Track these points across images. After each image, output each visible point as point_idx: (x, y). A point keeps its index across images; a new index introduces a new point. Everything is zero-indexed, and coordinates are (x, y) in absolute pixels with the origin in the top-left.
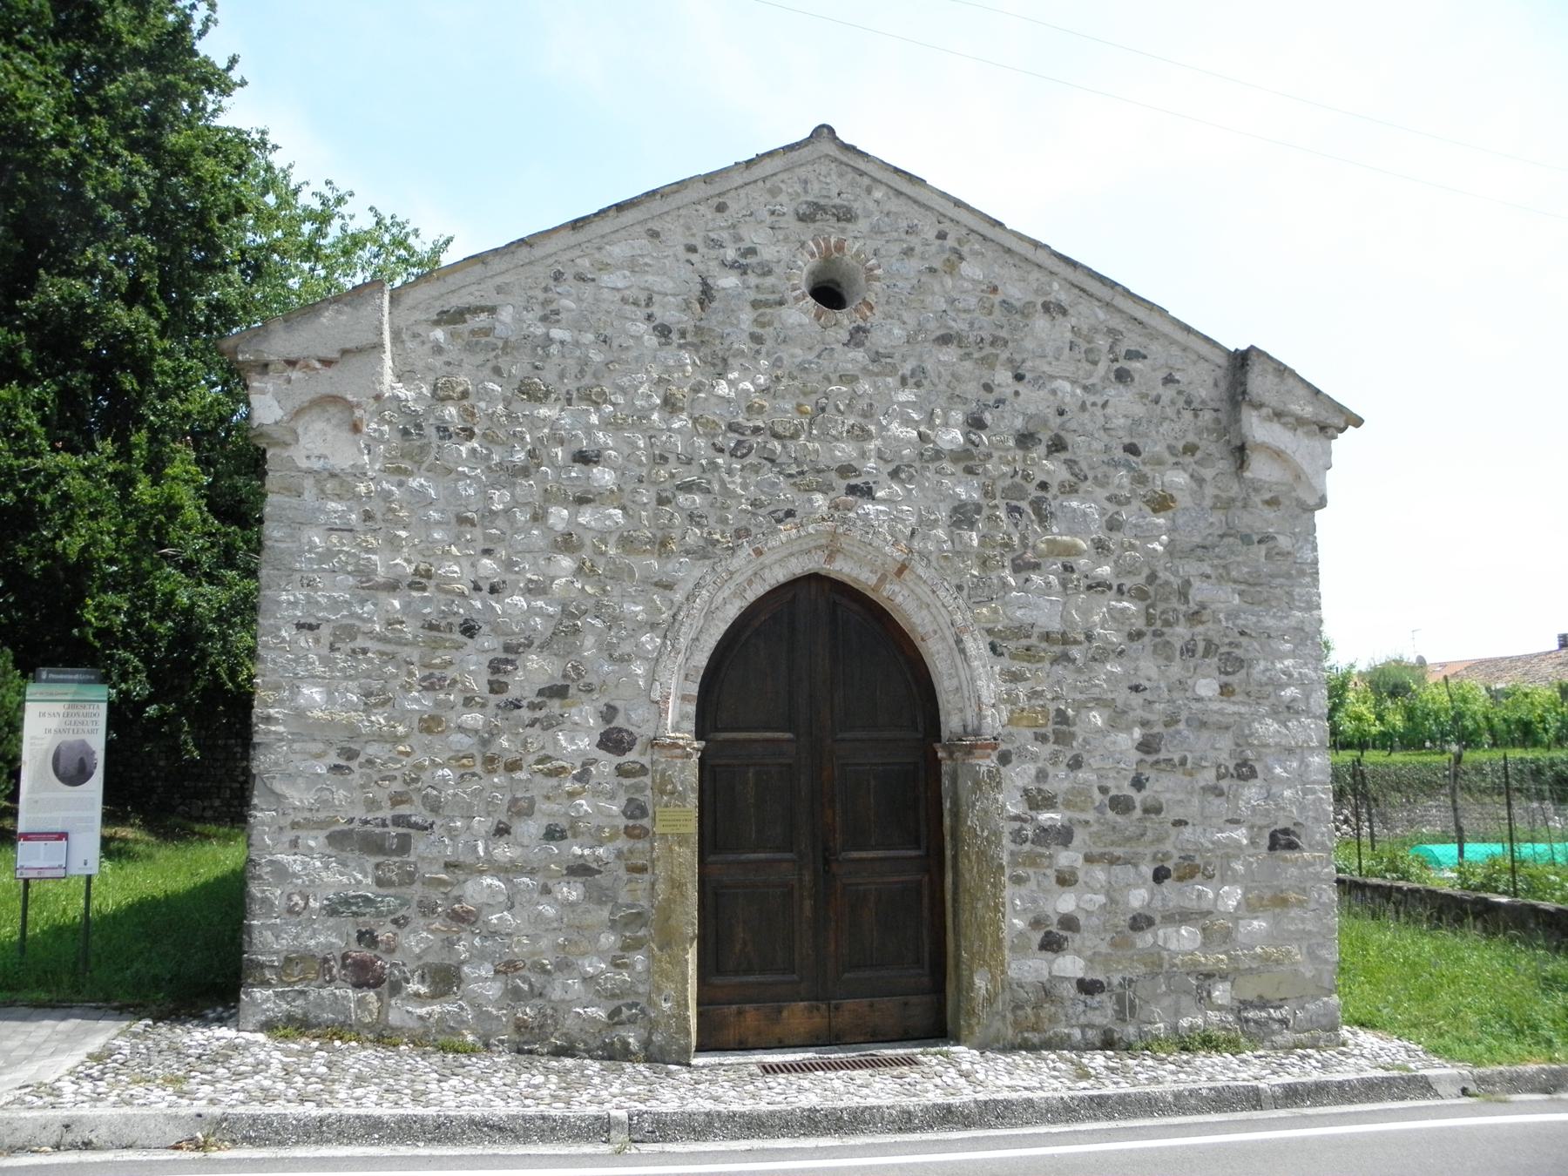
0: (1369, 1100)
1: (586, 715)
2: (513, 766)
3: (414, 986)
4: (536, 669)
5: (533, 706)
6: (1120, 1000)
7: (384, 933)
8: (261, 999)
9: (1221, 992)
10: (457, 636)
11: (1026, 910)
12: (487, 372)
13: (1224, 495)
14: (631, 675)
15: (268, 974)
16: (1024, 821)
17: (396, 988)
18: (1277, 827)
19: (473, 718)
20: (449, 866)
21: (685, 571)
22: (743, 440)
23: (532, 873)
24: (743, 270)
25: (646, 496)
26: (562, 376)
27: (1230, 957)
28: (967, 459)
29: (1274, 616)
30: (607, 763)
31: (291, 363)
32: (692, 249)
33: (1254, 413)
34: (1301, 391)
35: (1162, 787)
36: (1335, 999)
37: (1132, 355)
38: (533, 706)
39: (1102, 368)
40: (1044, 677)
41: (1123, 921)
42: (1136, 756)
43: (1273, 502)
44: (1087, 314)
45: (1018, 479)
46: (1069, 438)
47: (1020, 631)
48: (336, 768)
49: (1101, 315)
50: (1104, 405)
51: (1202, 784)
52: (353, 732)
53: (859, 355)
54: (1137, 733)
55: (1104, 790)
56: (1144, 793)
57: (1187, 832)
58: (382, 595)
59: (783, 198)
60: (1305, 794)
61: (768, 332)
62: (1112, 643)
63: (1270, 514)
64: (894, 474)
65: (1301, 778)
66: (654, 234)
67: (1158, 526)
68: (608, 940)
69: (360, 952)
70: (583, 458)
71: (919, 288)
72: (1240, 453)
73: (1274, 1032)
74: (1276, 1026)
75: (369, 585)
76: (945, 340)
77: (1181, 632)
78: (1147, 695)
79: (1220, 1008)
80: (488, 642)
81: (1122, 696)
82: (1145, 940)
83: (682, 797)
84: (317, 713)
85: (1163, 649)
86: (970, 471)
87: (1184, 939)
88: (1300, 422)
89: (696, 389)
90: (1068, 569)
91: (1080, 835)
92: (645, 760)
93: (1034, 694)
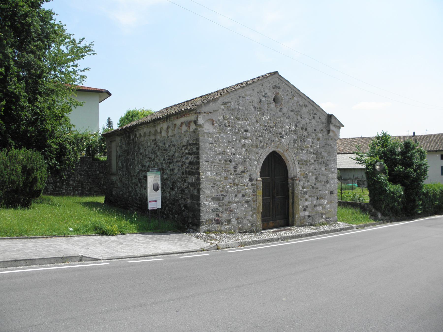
1: (247, 175)
2: (237, 185)
3: (225, 223)
4: (240, 168)
5: (240, 174)
7: (220, 215)
8: (203, 228)
10: (229, 162)
11: (303, 204)
12: (231, 114)
14: (253, 169)
15: (204, 223)
17: (222, 224)
19: (232, 177)
20: (229, 202)
21: (260, 150)
22: (267, 128)
23: (240, 203)
24: (265, 97)
25: (254, 138)
26: (242, 116)
28: (295, 132)
30: (250, 184)
31: (205, 112)
32: (258, 93)
35: (318, 185)
36: (337, 217)
37: (315, 114)
38: (240, 174)
39: (311, 116)
40: (304, 167)
41: (313, 206)
42: (315, 180)
43: (332, 139)
44: (310, 107)
46: (308, 128)
47: (302, 160)
48: (212, 186)
52: (215, 180)
53: (281, 113)
55: (311, 185)
58: (218, 155)
59: (271, 84)
61: (269, 109)
63: (331, 141)
64: (286, 134)
65: (334, 183)
66: (253, 90)
68: (251, 213)
69: (217, 218)
70: (246, 131)
71: (288, 102)
72: (329, 131)
75: (216, 154)
76: (292, 111)
80: (234, 163)
81: (313, 170)
82: (315, 209)
83: (260, 189)
84: (209, 177)
85: (318, 163)
86: (295, 134)
87: (320, 208)
89: (260, 119)
90: (308, 150)
91: (308, 193)
92: (255, 183)
93: (304, 170)
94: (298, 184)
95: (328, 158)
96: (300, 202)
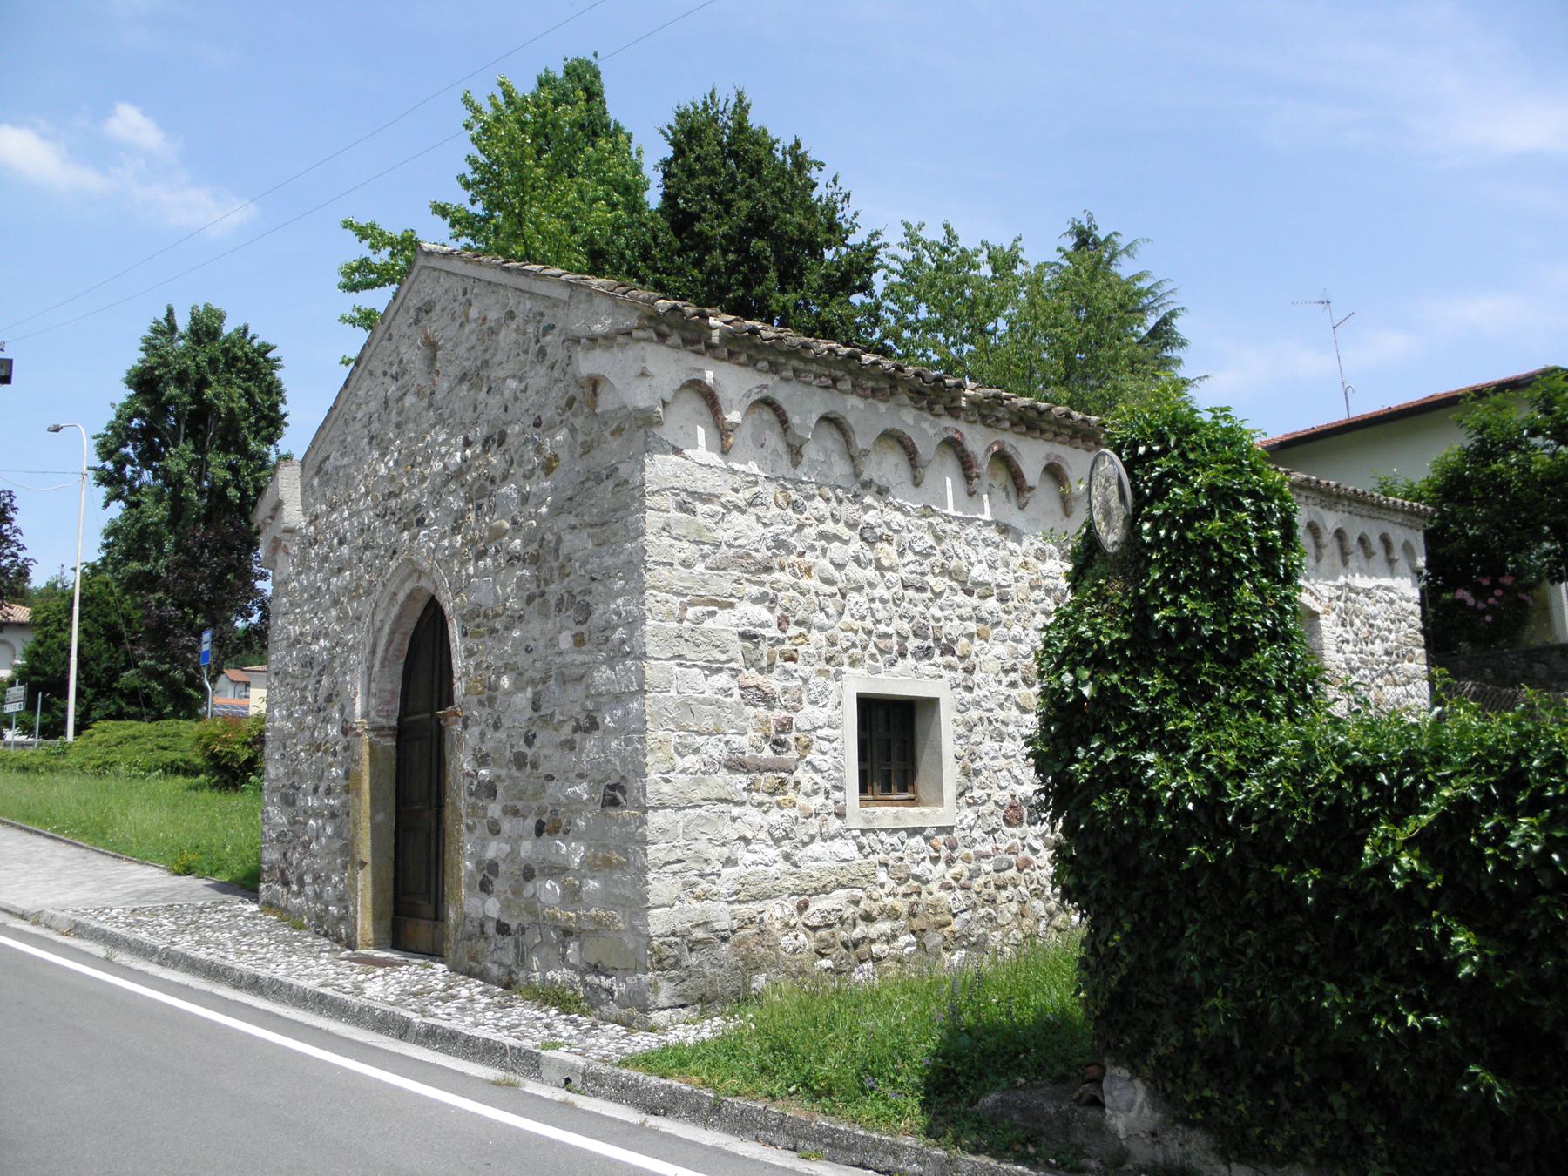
9: (572, 949)
18: (610, 782)
42: (529, 713)
43: (618, 431)
54: (529, 692)
56: (534, 749)
57: (552, 787)
77: (555, 589)
79: (572, 967)
81: (523, 660)
82: (529, 889)
87: (550, 889)
93: (478, 666)
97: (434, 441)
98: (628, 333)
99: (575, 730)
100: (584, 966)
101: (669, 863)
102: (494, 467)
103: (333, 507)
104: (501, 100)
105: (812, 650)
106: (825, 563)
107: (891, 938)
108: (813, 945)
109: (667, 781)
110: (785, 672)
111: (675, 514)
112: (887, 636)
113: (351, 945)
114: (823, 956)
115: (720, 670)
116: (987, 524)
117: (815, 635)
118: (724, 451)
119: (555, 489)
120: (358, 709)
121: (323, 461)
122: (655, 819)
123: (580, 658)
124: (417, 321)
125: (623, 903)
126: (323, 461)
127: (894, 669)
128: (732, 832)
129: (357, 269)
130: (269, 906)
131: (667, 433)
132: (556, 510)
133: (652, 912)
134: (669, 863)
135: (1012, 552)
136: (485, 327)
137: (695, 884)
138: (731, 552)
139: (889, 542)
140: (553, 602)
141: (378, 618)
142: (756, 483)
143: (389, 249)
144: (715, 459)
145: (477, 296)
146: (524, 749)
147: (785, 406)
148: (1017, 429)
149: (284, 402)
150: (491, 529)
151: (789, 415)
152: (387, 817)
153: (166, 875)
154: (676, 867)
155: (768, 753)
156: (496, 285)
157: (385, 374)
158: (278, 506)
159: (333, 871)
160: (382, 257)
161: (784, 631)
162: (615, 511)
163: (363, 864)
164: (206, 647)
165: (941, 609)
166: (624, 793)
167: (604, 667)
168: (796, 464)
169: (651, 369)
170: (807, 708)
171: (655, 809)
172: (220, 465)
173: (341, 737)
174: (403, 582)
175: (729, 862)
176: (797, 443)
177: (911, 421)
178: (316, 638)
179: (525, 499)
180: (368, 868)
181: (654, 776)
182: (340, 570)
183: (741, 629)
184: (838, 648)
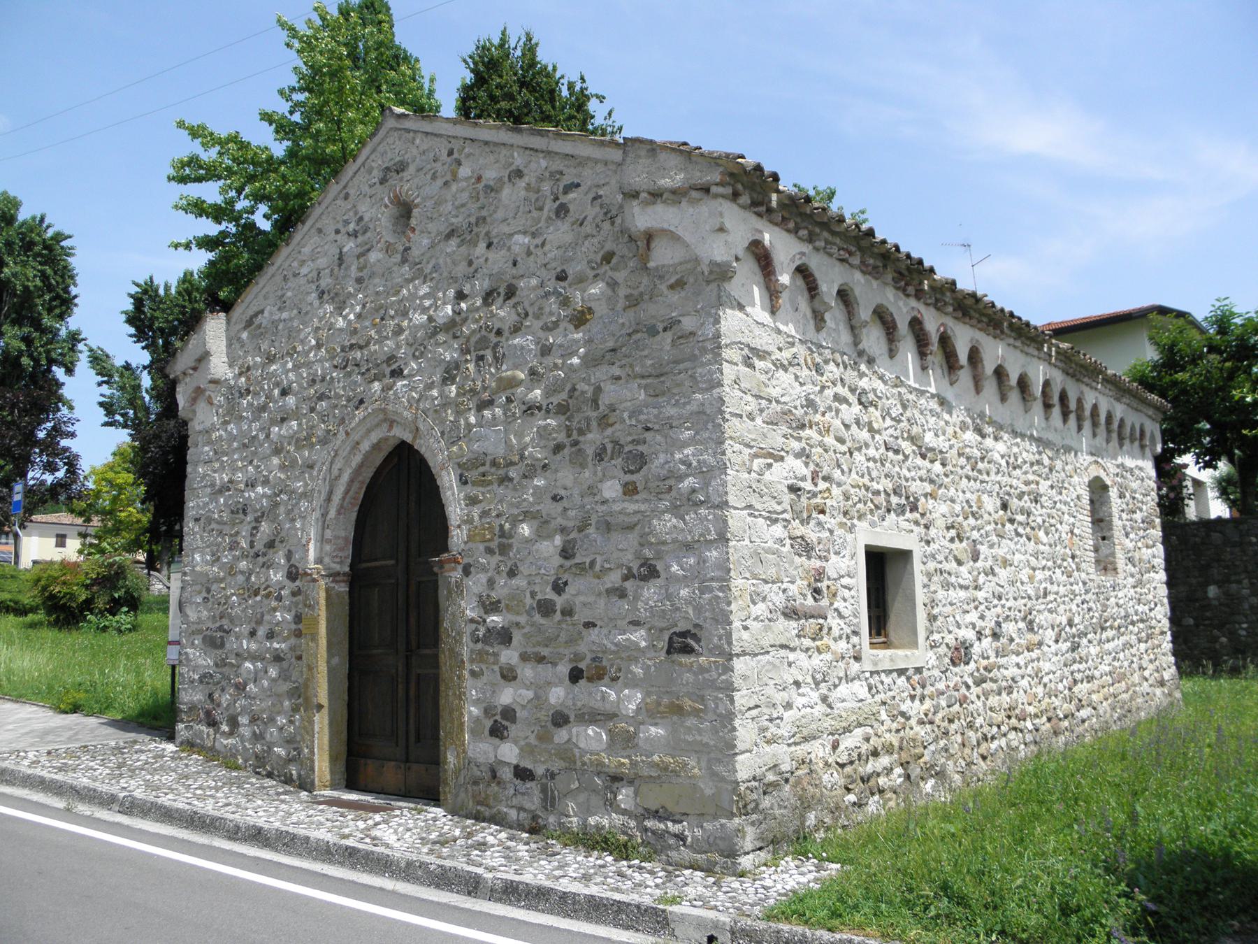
0: (588, 919)
5: (264, 555)
6: (544, 790)
9: (624, 796)
13: (636, 293)
16: (478, 623)
18: (677, 630)
27: (631, 760)
29: (677, 404)
33: (635, 203)
34: (673, 160)
42: (557, 560)
43: (679, 285)
45: (483, 332)
49: (544, 163)
50: (543, 244)
51: (609, 585)
54: (558, 540)
56: (565, 596)
57: (593, 634)
60: (702, 593)
62: (538, 459)
63: (674, 297)
67: (577, 341)
73: (670, 847)
74: (672, 841)
77: (593, 438)
78: (565, 503)
79: (624, 812)
81: (548, 507)
82: (562, 735)
85: (578, 460)
87: (592, 737)
88: (677, 195)
91: (517, 637)
93: (485, 514)
94: (459, 585)
95: (649, 414)
96: (469, 682)
97: (413, 296)
98: (706, 190)
99: (626, 578)
100: (641, 810)
101: (750, 709)
102: (501, 319)
103: (271, 359)
104: (319, 22)
105: (835, 504)
106: (837, 423)
107: (889, 771)
108: (842, 782)
109: (746, 628)
110: (819, 524)
111: (742, 368)
112: (877, 493)
113: (305, 784)
114: (848, 790)
115: (776, 521)
116: (933, 396)
117: (836, 491)
118: (773, 311)
119: (590, 341)
120: (312, 554)
121: (256, 315)
122: (739, 665)
123: (632, 507)
124: (383, 181)
125: (699, 749)
126: (256, 315)
127: (885, 523)
128: (789, 676)
129: (189, 164)
130: (190, 746)
131: (734, 288)
132: (591, 361)
133: (739, 758)
134: (750, 709)
135: (947, 423)
136: (480, 186)
137: (766, 729)
138: (779, 408)
139: (876, 406)
140: (590, 451)
141: (336, 467)
142: (793, 344)
143: (218, 148)
144: (765, 317)
145: (468, 156)
146: (551, 595)
147: (817, 275)
148: (955, 314)
149: (76, 285)
150: (500, 380)
151: (819, 282)
152: (342, 661)
153: (51, 713)
154: (754, 712)
155: (810, 601)
156: (496, 144)
157: (337, 232)
158: (204, 357)
159: (279, 713)
160: (210, 155)
161: (816, 485)
162: (677, 362)
163: (320, 707)
164: (17, 498)
165: (909, 470)
166: (698, 641)
167: (667, 516)
168: (819, 329)
169: (728, 225)
170: (834, 558)
171: (738, 655)
172: (14, 337)
173: (287, 583)
174: (369, 431)
175: (788, 706)
176: (822, 309)
177: (892, 299)
178: (251, 485)
179: (546, 351)
180: (325, 711)
181: (737, 624)
182: (283, 420)
183: (790, 482)
184: (850, 503)
